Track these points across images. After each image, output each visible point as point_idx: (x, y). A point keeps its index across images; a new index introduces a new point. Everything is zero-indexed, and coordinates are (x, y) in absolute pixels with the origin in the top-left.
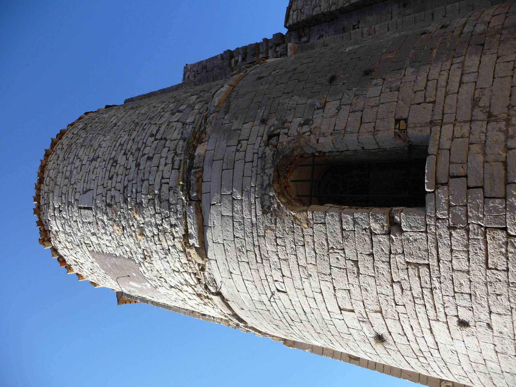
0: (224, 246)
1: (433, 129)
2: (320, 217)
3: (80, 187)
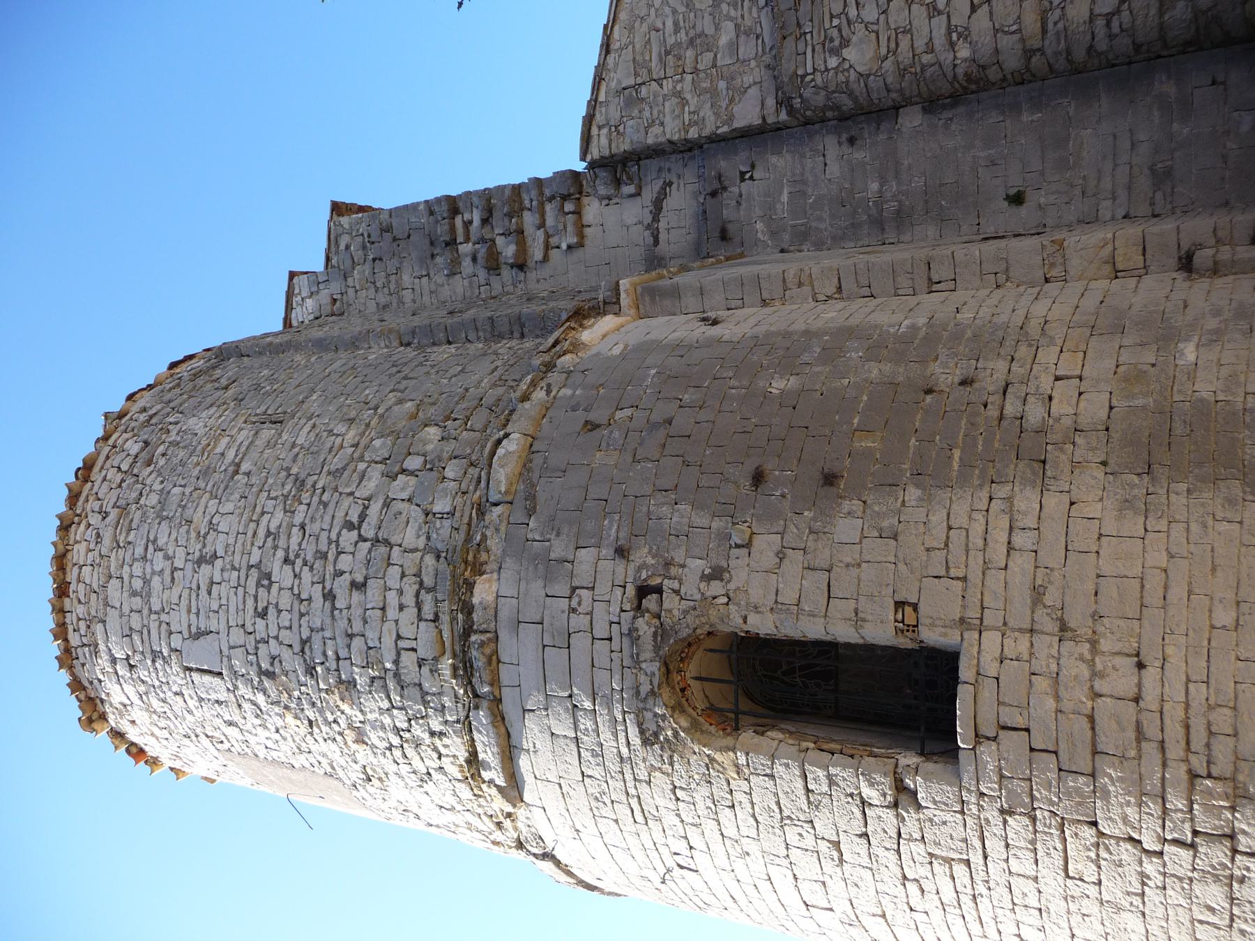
0: (561, 787)
1: (966, 635)
2: (763, 765)
3: (179, 620)
